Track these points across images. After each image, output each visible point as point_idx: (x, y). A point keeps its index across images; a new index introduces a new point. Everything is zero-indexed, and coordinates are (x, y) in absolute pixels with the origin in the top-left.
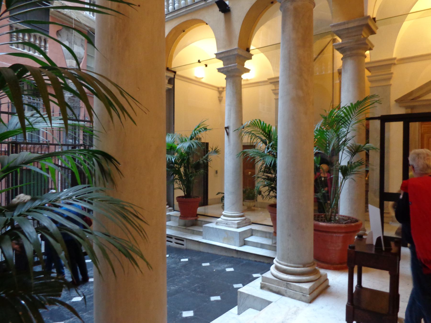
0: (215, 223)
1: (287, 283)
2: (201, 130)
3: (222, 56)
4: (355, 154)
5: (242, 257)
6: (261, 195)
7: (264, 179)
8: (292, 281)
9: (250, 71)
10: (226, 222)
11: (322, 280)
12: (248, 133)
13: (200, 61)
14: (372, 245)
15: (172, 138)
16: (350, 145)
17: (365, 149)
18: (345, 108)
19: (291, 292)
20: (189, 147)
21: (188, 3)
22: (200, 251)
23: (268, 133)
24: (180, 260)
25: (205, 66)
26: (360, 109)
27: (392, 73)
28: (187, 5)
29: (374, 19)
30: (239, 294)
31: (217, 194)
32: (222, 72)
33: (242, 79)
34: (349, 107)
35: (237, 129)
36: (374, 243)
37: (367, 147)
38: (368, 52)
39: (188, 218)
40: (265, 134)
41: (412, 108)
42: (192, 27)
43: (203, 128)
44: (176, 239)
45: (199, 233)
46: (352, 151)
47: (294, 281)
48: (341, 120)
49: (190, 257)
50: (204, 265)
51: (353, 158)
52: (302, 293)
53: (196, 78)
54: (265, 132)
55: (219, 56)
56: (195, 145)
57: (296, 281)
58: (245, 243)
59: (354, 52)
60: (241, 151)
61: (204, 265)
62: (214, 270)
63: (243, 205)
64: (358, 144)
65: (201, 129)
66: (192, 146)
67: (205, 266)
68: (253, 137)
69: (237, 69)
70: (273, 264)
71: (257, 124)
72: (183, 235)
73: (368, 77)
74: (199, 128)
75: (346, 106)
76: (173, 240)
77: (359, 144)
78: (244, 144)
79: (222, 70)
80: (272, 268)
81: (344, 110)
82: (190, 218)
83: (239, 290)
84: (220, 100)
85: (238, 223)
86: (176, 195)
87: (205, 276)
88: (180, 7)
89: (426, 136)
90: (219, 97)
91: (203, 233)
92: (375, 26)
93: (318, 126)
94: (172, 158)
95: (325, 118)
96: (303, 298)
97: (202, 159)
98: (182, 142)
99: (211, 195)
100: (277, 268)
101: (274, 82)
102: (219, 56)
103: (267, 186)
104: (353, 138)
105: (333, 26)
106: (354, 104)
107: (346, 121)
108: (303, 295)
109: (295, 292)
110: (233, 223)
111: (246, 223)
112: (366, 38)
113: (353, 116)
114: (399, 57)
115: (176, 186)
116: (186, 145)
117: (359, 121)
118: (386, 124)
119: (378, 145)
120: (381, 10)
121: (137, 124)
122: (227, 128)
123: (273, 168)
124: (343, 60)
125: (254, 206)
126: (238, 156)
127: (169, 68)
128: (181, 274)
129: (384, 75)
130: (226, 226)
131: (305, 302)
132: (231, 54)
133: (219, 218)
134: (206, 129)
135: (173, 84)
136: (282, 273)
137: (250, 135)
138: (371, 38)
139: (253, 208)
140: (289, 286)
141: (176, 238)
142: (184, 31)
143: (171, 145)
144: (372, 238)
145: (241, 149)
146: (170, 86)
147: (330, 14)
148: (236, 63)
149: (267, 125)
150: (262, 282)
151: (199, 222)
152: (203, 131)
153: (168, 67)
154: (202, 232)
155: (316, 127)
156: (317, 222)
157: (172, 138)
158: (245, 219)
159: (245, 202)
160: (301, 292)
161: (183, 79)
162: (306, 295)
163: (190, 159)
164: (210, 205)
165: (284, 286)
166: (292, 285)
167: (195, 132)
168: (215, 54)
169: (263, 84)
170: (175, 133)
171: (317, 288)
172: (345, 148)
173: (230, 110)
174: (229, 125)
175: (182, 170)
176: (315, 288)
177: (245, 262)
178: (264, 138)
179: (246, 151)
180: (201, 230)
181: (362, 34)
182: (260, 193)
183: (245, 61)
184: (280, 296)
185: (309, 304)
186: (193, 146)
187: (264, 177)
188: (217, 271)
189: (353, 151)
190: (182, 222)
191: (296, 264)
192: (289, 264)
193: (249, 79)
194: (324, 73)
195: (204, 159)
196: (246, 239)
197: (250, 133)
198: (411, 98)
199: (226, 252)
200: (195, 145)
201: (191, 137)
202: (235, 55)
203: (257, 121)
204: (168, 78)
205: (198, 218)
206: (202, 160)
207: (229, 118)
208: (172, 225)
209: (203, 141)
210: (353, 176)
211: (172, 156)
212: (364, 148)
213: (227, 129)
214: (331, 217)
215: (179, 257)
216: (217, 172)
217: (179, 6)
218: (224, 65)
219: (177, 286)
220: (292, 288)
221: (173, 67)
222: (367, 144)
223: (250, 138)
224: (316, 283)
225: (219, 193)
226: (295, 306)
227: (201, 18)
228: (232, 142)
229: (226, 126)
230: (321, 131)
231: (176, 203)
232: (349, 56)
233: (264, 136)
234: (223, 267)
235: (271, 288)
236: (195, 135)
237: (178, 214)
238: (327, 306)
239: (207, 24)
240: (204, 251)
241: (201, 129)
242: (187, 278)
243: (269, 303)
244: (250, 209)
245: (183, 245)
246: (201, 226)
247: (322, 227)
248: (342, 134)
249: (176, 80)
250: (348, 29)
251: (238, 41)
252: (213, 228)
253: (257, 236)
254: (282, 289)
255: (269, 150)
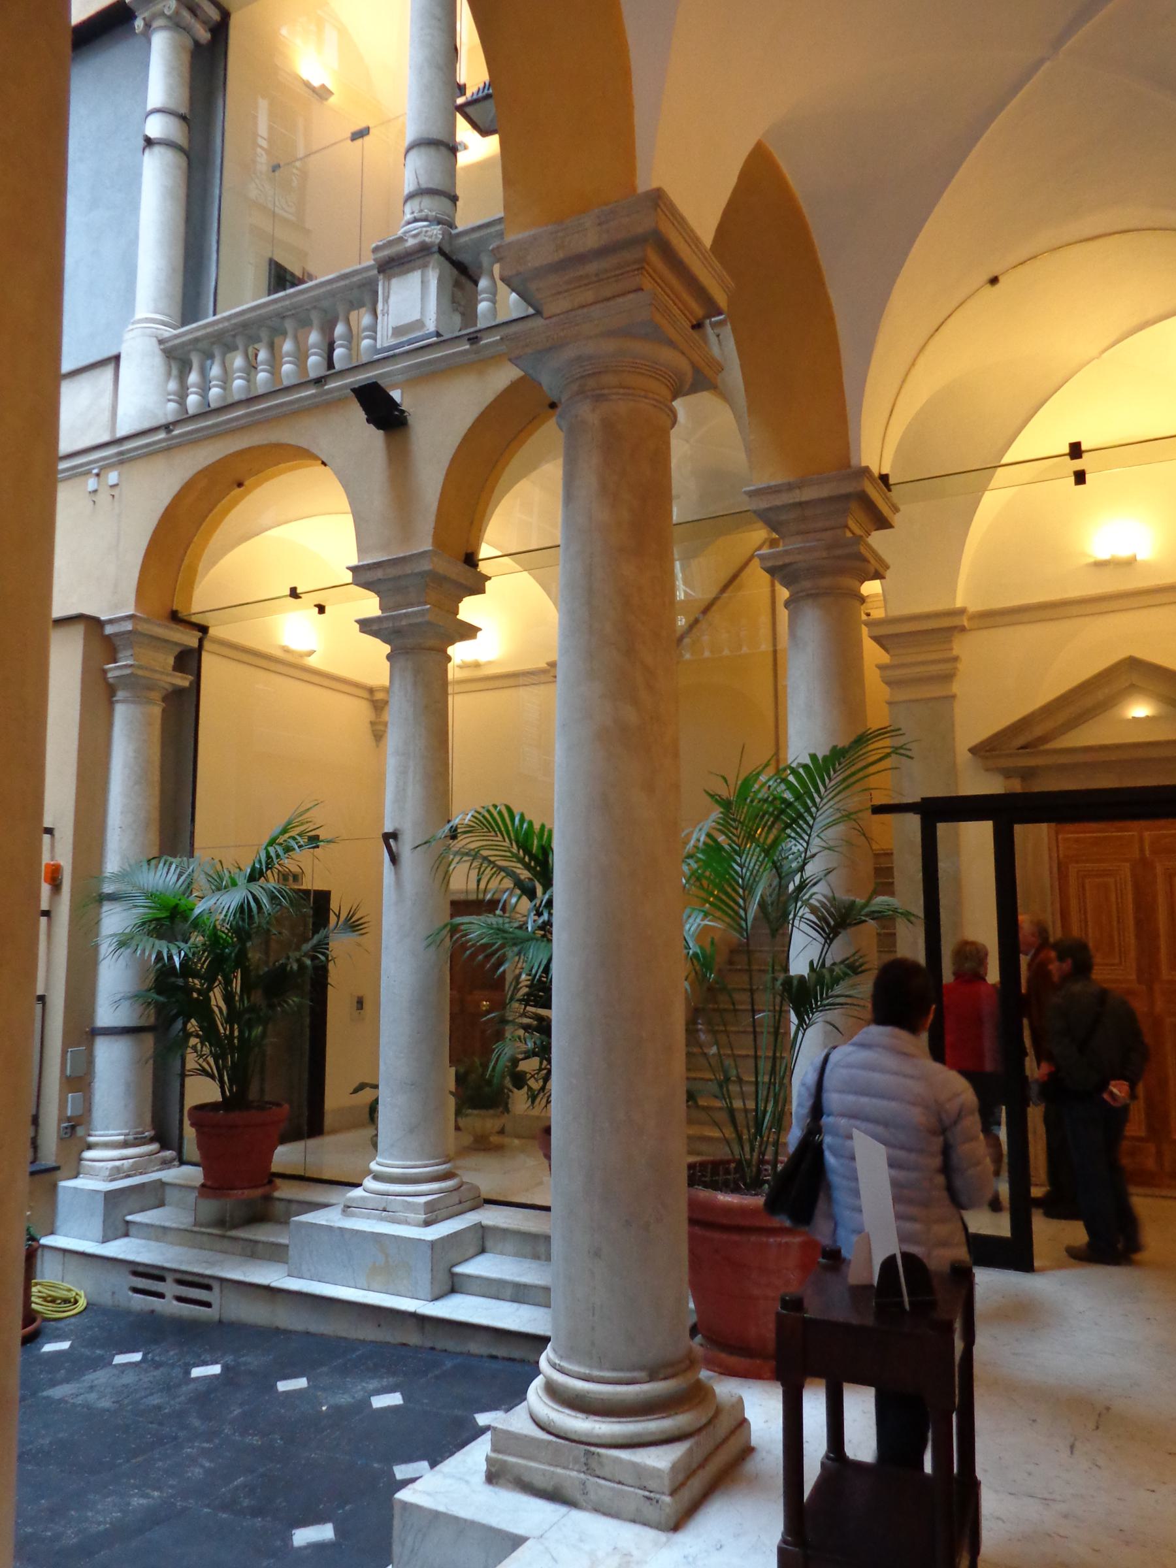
0: (339, 1208)
1: (587, 1453)
2: (293, 843)
3: (376, 578)
4: (836, 935)
5: (440, 1345)
6: (526, 1088)
7: (526, 1028)
8: (609, 1441)
9: (479, 634)
10: (381, 1201)
11: (724, 1424)
12: (467, 854)
13: (299, 591)
14: (872, 1286)
15: (180, 875)
16: (818, 901)
17: (875, 915)
18: (794, 772)
19: (602, 1488)
20: (243, 910)
21: (256, 388)
22: (277, 1329)
23: (540, 857)
24: (188, 1373)
25: (317, 609)
26: (848, 772)
27: (956, 659)
28: (254, 395)
29: (884, 478)
30: (397, 1511)
31: (356, 1091)
32: (375, 634)
33: (449, 659)
34: (805, 767)
35: (425, 843)
36: (875, 1283)
37: (873, 909)
38: (871, 588)
39: (231, 1192)
40: (530, 860)
41: (1027, 774)
42: (269, 471)
43: (300, 835)
44: (180, 1282)
45: (276, 1254)
46: (828, 924)
47: (614, 1441)
48: (782, 812)
49: (229, 1359)
50: (283, 1386)
51: (832, 946)
52: (644, 1488)
53: (286, 650)
54: (527, 851)
55: (363, 576)
56: (265, 900)
57: (620, 1441)
58: (454, 1286)
59: (826, 582)
60: (442, 924)
61: (283, 1386)
62: (324, 1408)
63: (457, 1128)
64: (844, 897)
65: (294, 838)
66: (253, 904)
67: (287, 1393)
68: (488, 872)
69: (429, 623)
70: (537, 1372)
71: (485, 822)
72: (212, 1264)
73: (881, 667)
74: (287, 835)
75: (794, 765)
76: (169, 1288)
77: (852, 898)
78: (456, 897)
79: (375, 627)
80: (535, 1389)
81: (791, 778)
82: (240, 1192)
83: (403, 1495)
84: (378, 735)
85: (426, 1203)
86: (190, 1101)
87: (281, 1439)
88: (230, 401)
89: (1073, 869)
90: (372, 723)
91: (292, 1252)
92: (887, 499)
93: (698, 837)
94: (174, 951)
95: (726, 805)
96: (650, 1511)
97: (297, 954)
98: (219, 887)
99: (336, 1096)
100: (554, 1392)
101: (545, 674)
102: (363, 576)
103: (535, 1054)
104: (826, 875)
105: (752, 494)
106: (820, 757)
107: (801, 816)
108: (649, 1498)
109: (620, 1486)
110: (408, 1203)
111: (460, 1202)
112: (858, 539)
113: (822, 798)
114: (973, 608)
115: (191, 1062)
116: (231, 900)
117: (848, 816)
118: (942, 828)
119: (917, 907)
120: (906, 451)
121: (705, 794)
122: (390, 837)
123: (541, 993)
124: (791, 607)
125: (502, 1132)
126: (432, 940)
127: (183, 614)
128: (181, 1434)
129: (933, 662)
130: (382, 1219)
131: (658, 1527)
132: (408, 570)
133: (359, 1185)
134: (314, 841)
135: (196, 672)
136: (567, 1411)
137: (475, 864)
138: (877, 539)
139: (495, 1139)
140: (594, 1464)
141: (179, 1276)
142: (240, 485)
143: (173, 902)
144: (870, 1260)
145: (444, 916)
146: (182, 678)
147: (741, 457)
148: (426, 603)
149: (537, 827)
150: (494, 1455)
151: (279, 1208)
152: (300, 847)
153: (175, 608)
154: (287, 1246)
155: (695, 836)
156: (704, 1194)
157: (180, 875)
158: (457, 1189)
159: (467, 1115)
160: (639, 1488)
161: (244, 657)
162: (658, 1496)
163: (250, 955)
164: (334, 1131)
165: (577, 1467)
166: (608, 1457)
167: (268, 853)
168: (349, 568)
169: (511, 682)
170: (197, 853)
171: (701, 1466)
172: (805, 911)
173: (403, 772)
174: (397, 826)
175: (217, 998)
176: (694, 1466)
177: (449, 1364)
178: (525, 874)
179: (462, 924)
180: (284, 1240)
181: (847, 526)
182: (519, 1080)
183: (461, 600)
184: (562, 1510)
185: (670, 1535)
186: (259, 907)
187: (526, 1021)
188: (337, 1409)
189: (832, 923)
190: (210, 1207)
191: (621, 1370)
192: (596, 1373)
193: (482, 659)
194: (745, 649)
195: (306, 955)
196: (459, 1269)
197: (474, 855)
198: (1021, 740)
199: (597, 1254)
200: (265, 900)
201: (253, 869)
202: (422, 574)
203: (500, 813)
204: (177, 650)
205: (276, 1189)
206: (298, 961)
207: (400, 798)
208: (167, 1224)
209: (306, 885)
210: (834, 1015)
211: (171, 946)
212: (867, 910)
213: (391, 841)
214: (759, 1171)
215: (188, 1359)
216: (360, 1003)
217: (224, 397)
218: (381, 608)
219: (156, 1494)
220: (606, 1472)
221: (195, 608)
222: (880, 899)
223: (474, 874)
224: (697, 1444)
225: (361, 1087)
226: (615, 1548)
227: (303, 443)
228: (409, 888)
229: (388, 828)
230: (713, 848)
231: (190, 1132)
232: (809, 596)
233: (527, 867)
234: (362, 1393)
235: (526, 1478)
236: (267, 864)
237: (193, 1174)
238: (737, 1536)
239: (324, 464)
240: (291, 1327)
241: (294, 838)
242: (205, 1452)
243: (516, 1542)
244: (482, 1145)
245: (208, 1305)
246: (284, 1221)
247: (727, 1210)
248: (792, 861)
249: (206, 658)
250: (800, 504)
251: (435, 528)
252: (330, 1229)
253: (502, 1253)
254: (570, 1476)
255: (541, 921)
